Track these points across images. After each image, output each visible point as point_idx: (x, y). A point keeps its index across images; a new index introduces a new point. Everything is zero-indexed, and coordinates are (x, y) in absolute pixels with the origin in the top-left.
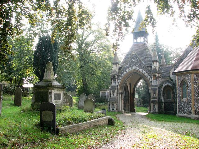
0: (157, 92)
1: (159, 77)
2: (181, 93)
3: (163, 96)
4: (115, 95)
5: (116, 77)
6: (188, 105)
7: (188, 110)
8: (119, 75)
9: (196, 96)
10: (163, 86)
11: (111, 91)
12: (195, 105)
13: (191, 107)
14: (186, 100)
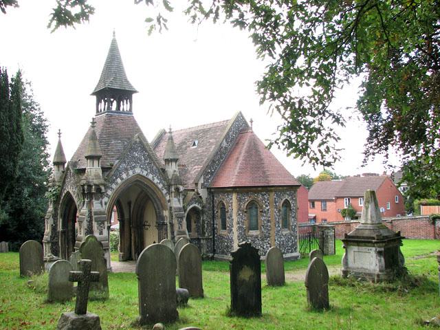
6: (263, 240)
10: (188, 209)
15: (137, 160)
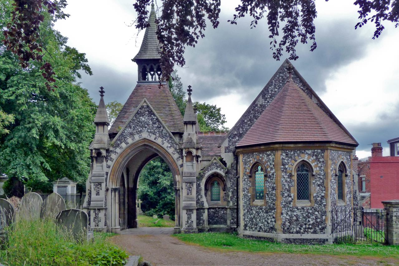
1: (197, 157)
2: (251, 189)
3: (206, 194)
4: (102, 192)
5: (104, 153)
6: (267, 212)
7: (268, 223)
8: (111, 149)
9: (286, 195)
11: (92, 184)
13: (273, 218)
14: (263, 203)
15: (144, 125)
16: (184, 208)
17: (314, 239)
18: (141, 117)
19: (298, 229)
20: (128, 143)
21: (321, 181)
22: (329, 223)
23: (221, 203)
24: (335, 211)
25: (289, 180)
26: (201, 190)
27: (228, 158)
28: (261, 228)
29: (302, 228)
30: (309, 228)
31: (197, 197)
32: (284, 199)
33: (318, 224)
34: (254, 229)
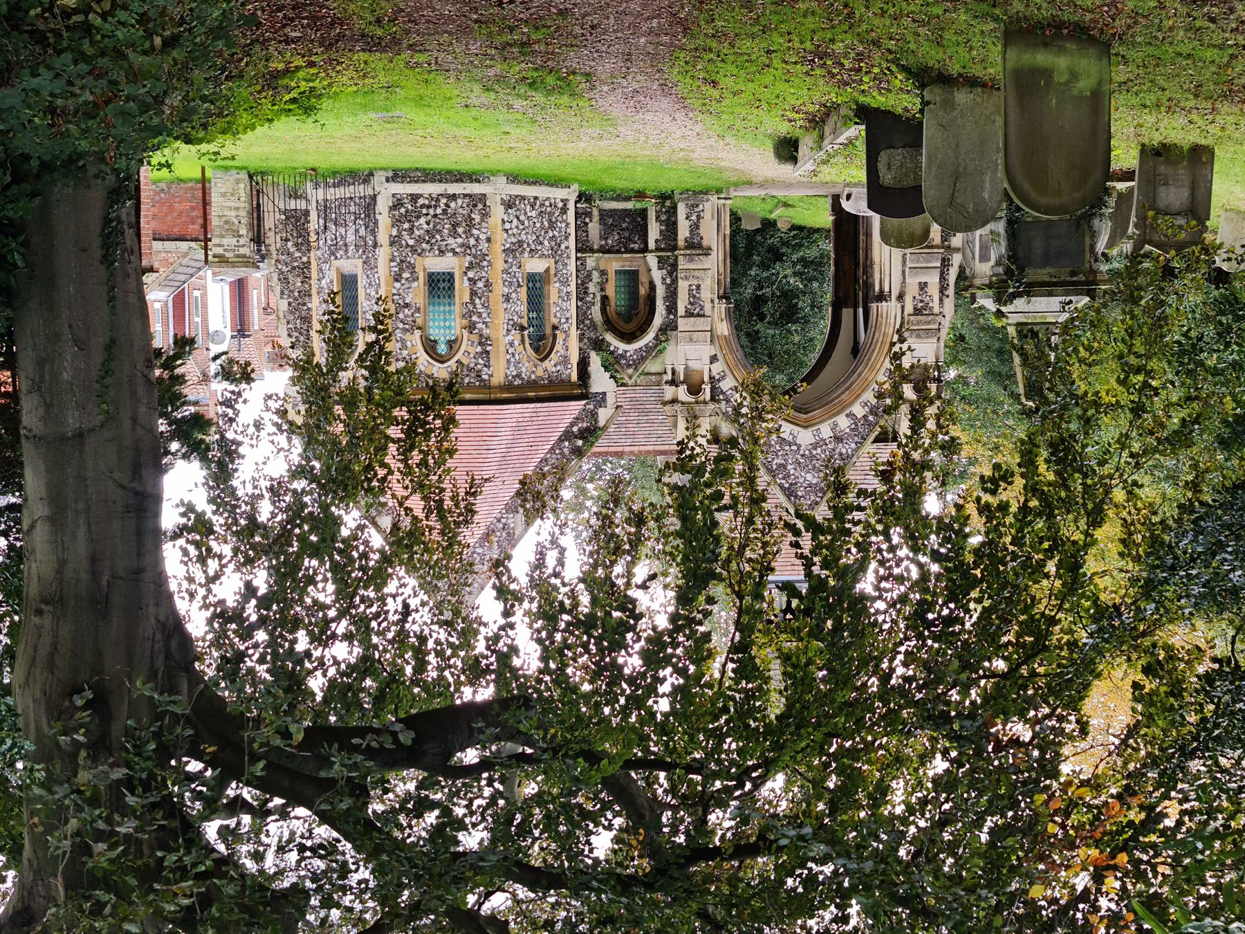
0: (682, 305)
1: (673, 382)
3: (652, 287)
4: (912, 290)
6: (520, 243)
7: (518, 218)
9: (480, 284)
11: (936, 310)
12: (489, 240)
13: (507, 231)
16: (707, 252)
17: (416, 182)
18: (814, 481)
19: (453, 205)
20: (847, 416)
21: (401, 316)
22: (384, 219)
23: (614, 264)
24: (367, 248)
25: (475, 318)
26: (666, 299)
27: (601, 381)
28: (533, 206)
29: (443, 206)
30: (429, 207)
31: (675, 281)
32: (484, 274)
33: (407, 217)
34: (547, 203)
